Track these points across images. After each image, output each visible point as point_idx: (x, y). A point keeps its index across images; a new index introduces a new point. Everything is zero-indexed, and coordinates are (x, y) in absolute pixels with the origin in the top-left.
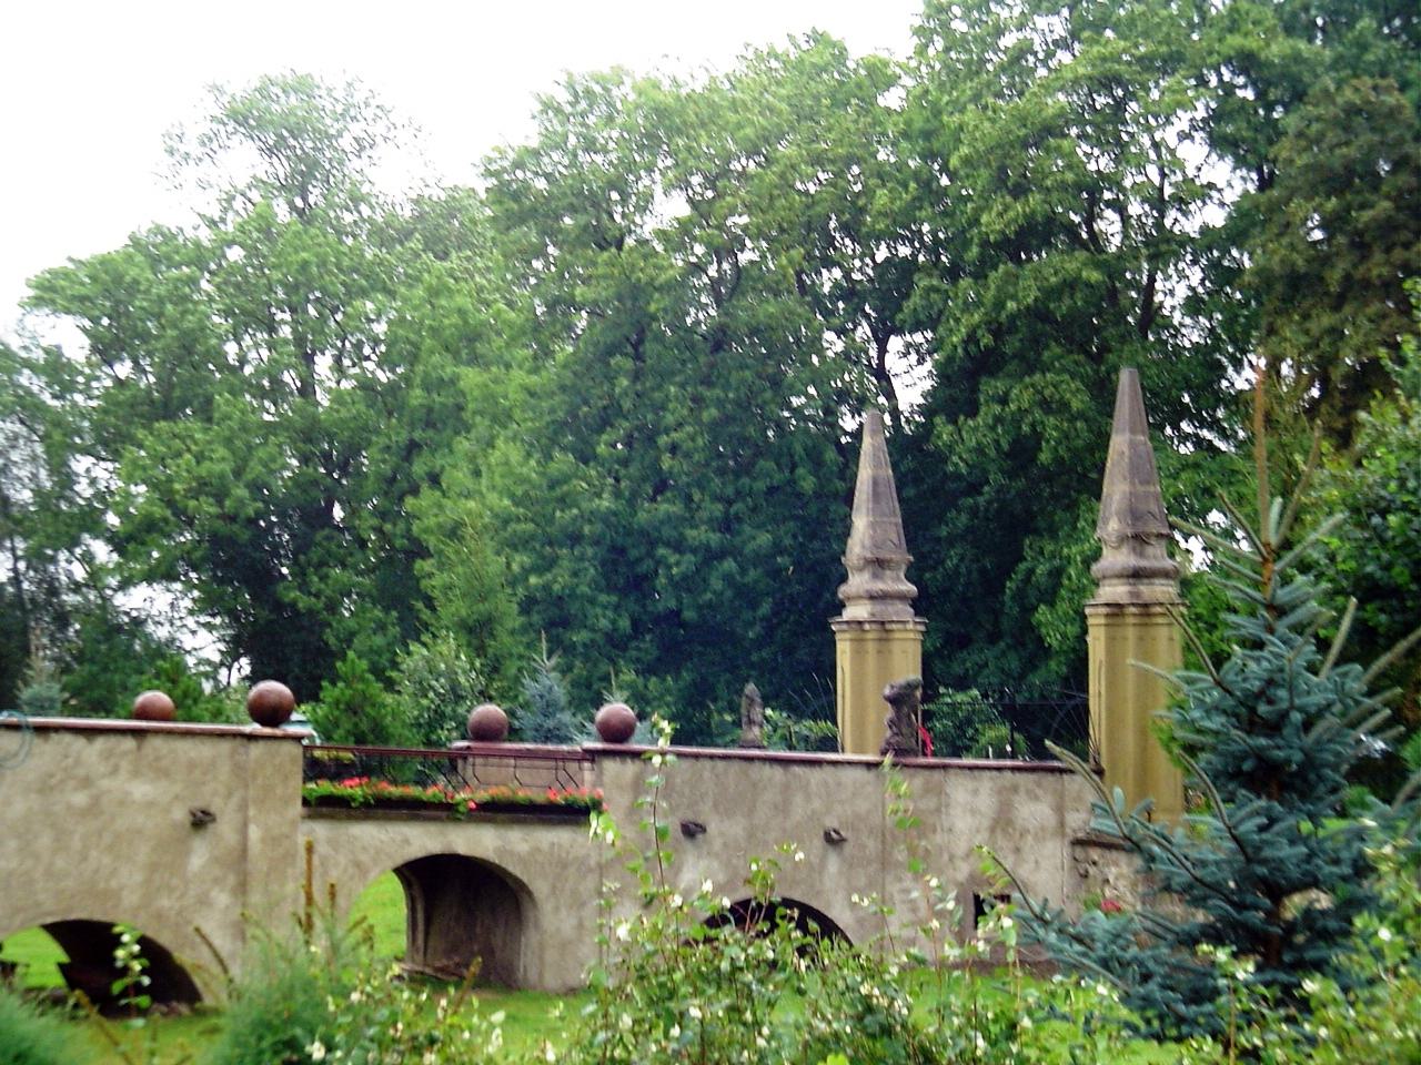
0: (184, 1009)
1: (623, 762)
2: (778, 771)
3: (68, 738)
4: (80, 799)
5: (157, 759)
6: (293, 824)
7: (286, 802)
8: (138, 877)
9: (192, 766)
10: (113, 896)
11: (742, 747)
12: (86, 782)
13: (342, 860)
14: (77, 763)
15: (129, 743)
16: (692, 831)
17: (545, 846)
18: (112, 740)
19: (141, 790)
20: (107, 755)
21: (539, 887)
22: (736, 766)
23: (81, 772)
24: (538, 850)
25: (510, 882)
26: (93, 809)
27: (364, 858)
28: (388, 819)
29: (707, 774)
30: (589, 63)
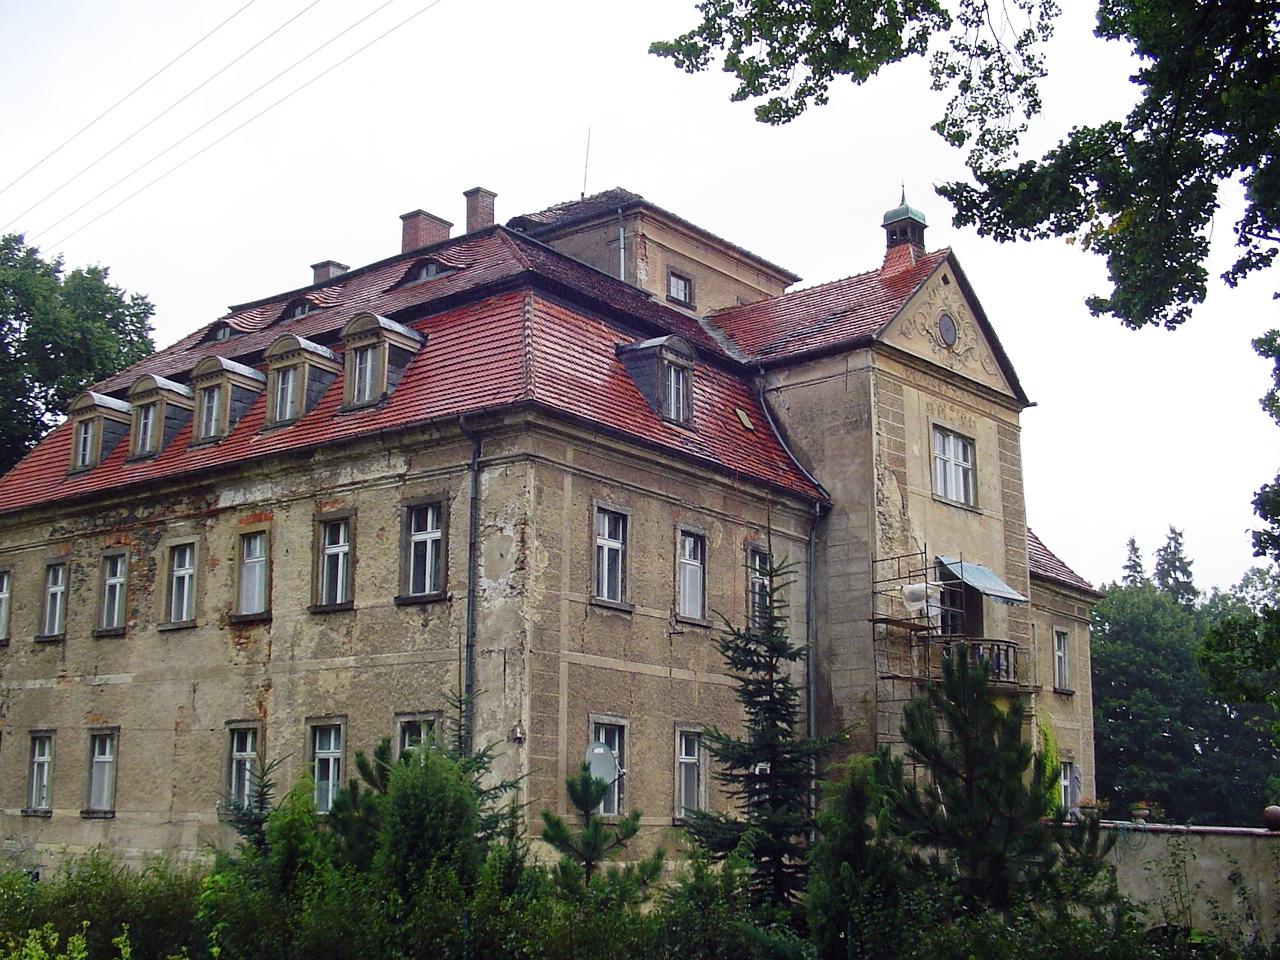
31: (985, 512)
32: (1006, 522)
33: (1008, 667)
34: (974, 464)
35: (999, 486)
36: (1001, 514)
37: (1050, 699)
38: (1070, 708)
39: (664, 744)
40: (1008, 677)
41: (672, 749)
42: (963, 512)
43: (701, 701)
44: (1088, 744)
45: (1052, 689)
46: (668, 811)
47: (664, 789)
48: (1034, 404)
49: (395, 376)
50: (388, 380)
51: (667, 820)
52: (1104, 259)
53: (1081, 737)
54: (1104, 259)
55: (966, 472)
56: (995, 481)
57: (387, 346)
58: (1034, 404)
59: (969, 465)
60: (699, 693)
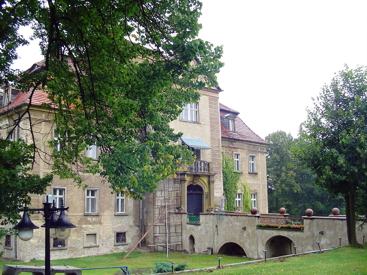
0: (245, 257)
1: (307, 220)
2: (341, 221)
3: (229, 216)
4: (231, 225)
5: (239, 219)
6: (255, 230)
7: (254, 226)
8: (238, 237)
9: (243, 220)
10: (235, 239)
11: (349, 205)
12: (232, 223)
13: (264, 236)
14: (230, 220)
15: (236, 217)
16: (322, 233)
17: (296, 235)
18: (234, 216)
19: (237, 224)
20: (234, 219)
21: (295, 241)
22: (331, 221)
23: (231, 221)
24: (294, 236)
25: (65, 227)
26: (232, 227)
27: (267, 236)
28: (270, 229)
29: (325, 222)
30: (284, 130)
31: (202, 123)
32: (211, 125)
33: (201, 168)
34: (198, 109)
35: (209, 115)
36: (209, 123)
37: (247, 176)
38: (256, 178)
39: (81, 193)
40: (201, 171)
41: (84, 195)
42: (193, 124)
43: (96, 181)
44: (264, 188)
45: (248, 172)
46: (83, 211)
47: (81, 206)
48: (223, 91)
49: (14, 97)
50: (11, 98)
51: (83, 214)
52: (202, 35)
53: (261, 186)
54: (202, 35)
55: (197, 112)
56: (208, 114)
57: (11, 89)
58: (223, 91)
59: (197, 110)
60: (95, 179)
